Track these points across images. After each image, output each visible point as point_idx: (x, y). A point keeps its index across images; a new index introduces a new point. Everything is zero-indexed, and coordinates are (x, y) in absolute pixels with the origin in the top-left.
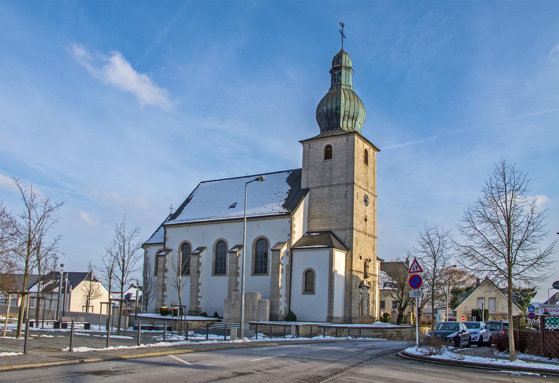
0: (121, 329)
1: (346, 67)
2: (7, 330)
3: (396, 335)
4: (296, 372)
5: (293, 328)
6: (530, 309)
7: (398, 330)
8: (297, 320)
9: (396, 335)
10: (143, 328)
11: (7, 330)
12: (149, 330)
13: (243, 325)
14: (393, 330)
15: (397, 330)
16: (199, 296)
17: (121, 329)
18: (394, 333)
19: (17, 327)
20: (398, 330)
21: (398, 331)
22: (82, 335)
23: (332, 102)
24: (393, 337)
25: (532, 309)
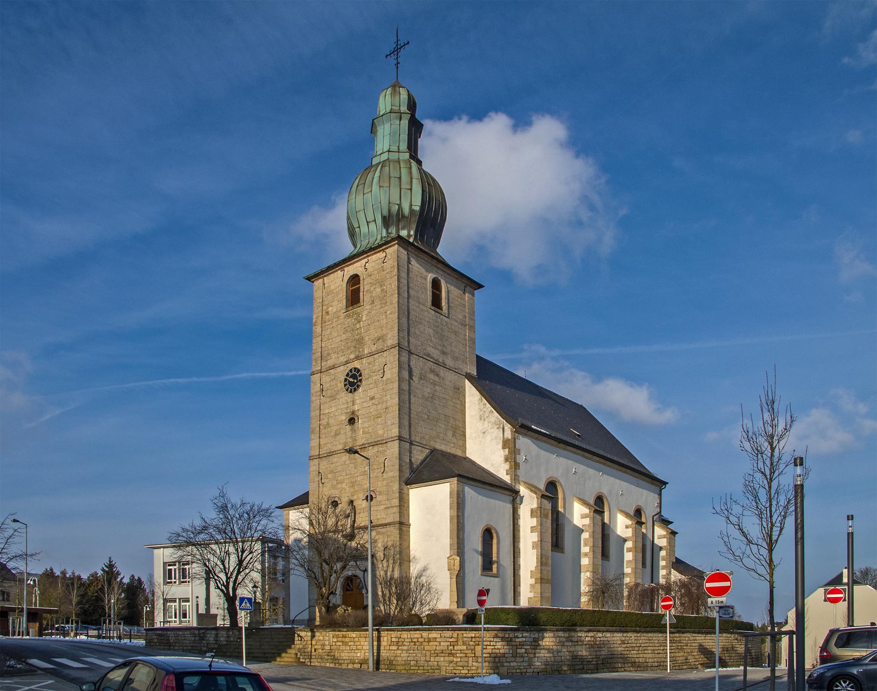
0: (111, 635)
1: (400, 151)
2: (187, 568)
3: (156, 640)
4: (445, 637)
5: (719, 570)
6: (243, 605)
7: (160, 632)
8: (29, 623)
9: (156, 640)
10: (110, 634)
11: (187, 568)
12: (284, 625)
13: (28, 637)
14: (153, 632)
15: (158, 632)
16: (665, 561)
17: (111, 635)
18: (153, 637)
19: (787, 672)
20: (160, 632)
21: (159, 635)
22: (580, 595)
23: (364, 192)
24: (153, 644)
25: (248, 605)
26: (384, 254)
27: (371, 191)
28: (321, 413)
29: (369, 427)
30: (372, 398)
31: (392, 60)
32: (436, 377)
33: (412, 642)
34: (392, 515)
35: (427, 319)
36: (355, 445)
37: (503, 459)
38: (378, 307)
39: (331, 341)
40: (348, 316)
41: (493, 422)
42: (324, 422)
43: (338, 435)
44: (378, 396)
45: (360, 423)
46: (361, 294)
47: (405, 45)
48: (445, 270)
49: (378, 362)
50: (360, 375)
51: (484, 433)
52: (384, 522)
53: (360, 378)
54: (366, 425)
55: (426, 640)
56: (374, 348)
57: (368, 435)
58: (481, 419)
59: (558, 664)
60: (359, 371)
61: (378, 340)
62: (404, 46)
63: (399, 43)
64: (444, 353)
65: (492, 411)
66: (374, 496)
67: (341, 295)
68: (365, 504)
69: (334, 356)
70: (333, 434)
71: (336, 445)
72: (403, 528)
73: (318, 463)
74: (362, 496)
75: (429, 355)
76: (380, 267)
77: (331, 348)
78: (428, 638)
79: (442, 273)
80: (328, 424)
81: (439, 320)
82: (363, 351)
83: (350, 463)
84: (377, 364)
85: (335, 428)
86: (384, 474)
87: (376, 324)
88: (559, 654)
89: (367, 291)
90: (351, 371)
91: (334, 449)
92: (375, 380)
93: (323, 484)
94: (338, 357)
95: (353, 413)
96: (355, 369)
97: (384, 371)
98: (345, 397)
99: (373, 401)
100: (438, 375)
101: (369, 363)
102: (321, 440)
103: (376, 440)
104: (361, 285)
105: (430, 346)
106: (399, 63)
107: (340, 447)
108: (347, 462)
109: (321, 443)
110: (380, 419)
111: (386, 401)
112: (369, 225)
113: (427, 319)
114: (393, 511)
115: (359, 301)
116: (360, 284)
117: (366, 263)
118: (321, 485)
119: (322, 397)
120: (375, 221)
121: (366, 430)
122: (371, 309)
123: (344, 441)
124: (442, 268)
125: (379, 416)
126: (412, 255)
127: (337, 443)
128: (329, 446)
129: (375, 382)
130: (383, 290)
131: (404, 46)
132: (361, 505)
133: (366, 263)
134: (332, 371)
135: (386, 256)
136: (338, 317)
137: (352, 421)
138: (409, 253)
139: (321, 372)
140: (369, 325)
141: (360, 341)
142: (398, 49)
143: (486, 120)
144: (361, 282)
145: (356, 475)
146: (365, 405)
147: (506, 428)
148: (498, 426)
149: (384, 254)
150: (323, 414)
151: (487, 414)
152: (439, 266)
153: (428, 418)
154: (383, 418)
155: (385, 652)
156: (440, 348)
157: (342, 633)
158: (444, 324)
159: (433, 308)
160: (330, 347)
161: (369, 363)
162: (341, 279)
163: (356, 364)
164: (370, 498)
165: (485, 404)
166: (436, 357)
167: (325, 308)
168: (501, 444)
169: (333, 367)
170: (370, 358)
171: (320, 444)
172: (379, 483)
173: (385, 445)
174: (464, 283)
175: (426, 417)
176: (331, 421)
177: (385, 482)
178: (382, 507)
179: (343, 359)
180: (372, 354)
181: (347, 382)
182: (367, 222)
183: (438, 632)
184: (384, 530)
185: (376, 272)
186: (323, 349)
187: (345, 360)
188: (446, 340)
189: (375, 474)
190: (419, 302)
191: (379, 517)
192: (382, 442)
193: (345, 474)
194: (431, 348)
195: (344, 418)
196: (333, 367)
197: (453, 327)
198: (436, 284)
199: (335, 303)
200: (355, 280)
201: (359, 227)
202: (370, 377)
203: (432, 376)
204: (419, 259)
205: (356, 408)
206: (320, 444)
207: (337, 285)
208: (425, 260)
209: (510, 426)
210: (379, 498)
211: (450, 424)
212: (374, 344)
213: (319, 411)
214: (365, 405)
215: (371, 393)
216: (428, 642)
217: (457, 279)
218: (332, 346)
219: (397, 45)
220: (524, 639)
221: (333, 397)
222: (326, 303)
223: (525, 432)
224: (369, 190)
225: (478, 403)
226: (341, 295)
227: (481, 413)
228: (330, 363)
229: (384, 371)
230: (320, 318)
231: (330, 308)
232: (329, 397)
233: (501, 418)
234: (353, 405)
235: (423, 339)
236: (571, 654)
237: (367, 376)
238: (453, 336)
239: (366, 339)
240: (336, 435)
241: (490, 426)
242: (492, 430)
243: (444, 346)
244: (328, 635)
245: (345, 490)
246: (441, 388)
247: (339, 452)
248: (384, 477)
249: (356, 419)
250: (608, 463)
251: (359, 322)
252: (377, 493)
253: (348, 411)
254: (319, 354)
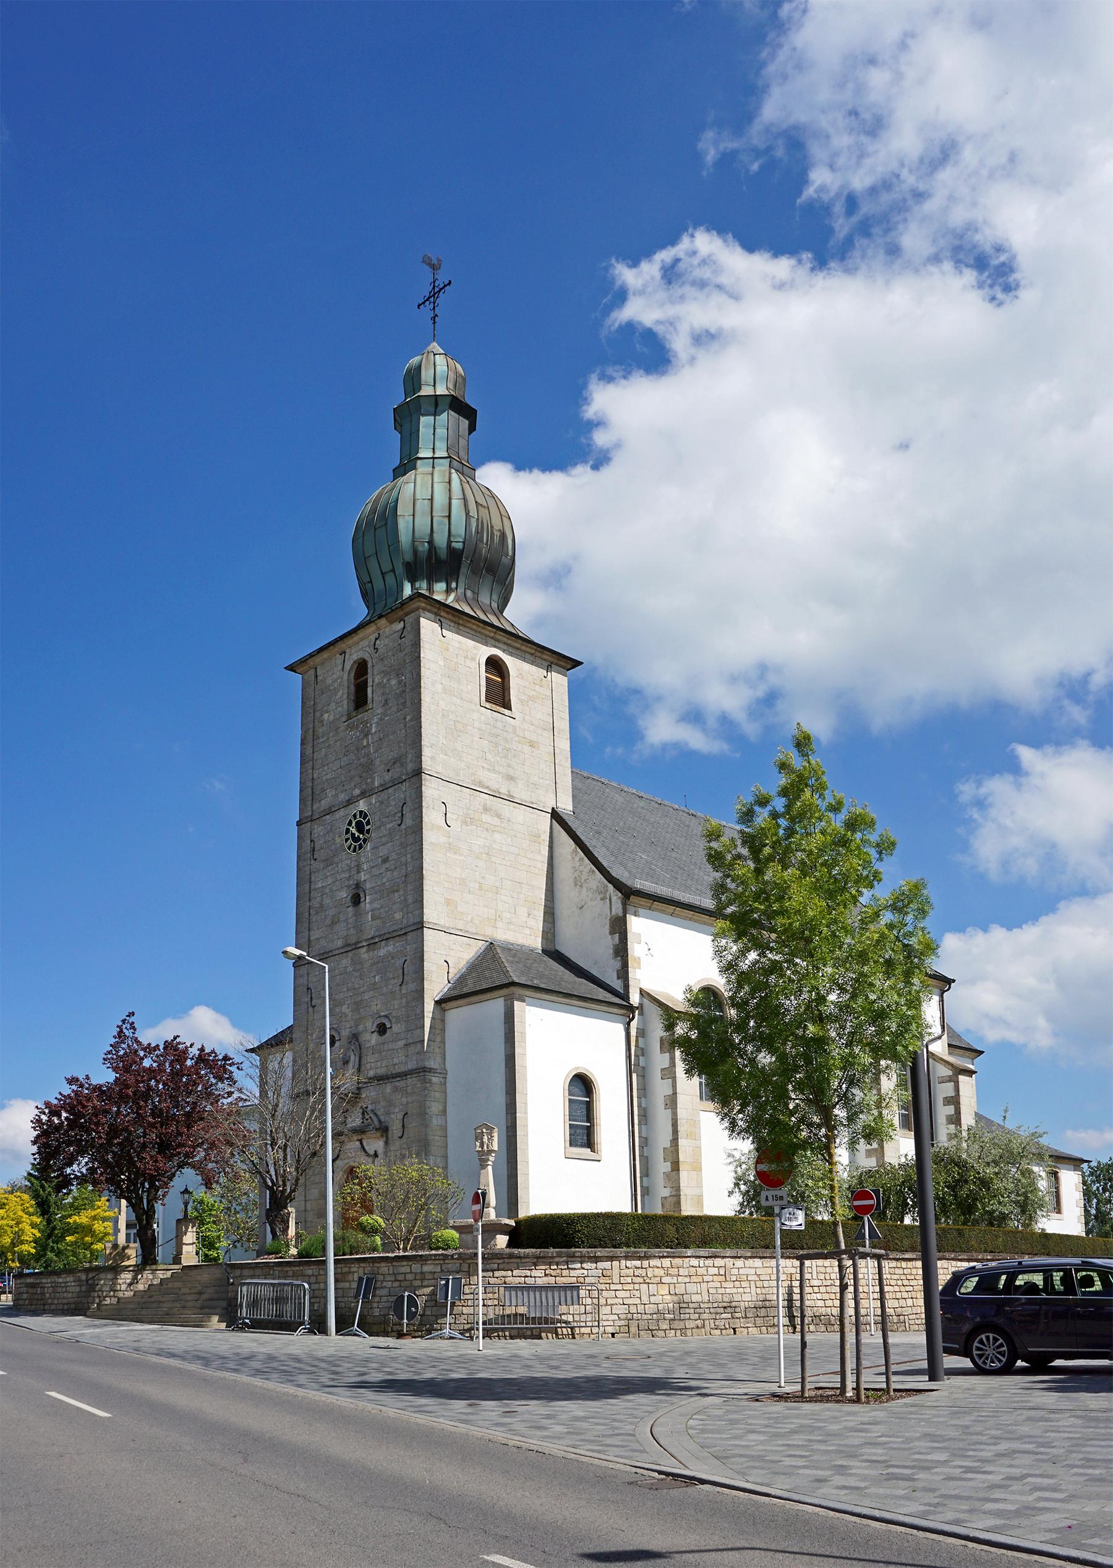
26: (402, 624)
27: (386, 524)
28: (312, 887)
29: (382, 907)
30: (385, 860)
31: (427, 311)
32: (496, 819)
33: (396, 1280)
34: (414, 1058)
35: (476, 724)
36: (360, 939)
37: (611, 951)
38: (394, 709)
39: (326, 768)
40: (351, 727)
41: (595, 888)
42: (315, 903)
43: (336, 923)
44: (394, 856)
45: (367, 903)
46: (369, 690)
47: (445, 286)
48: (509, 642)
49: (394, 800)
50: (368, 823)
51: (581, 908)
52: (403, 1069)
53: (367, 828)
54: (376, 905)
55: (418, 1277)
56: (387, 777)
57: (378, 922)
58: (576, 885)
59: (650, 1317)
60: (366, 816)
61: (394, 763)
62: (443, 288)
63: (436, 285)
64: (511, 778)
65: (593, 871)
66: (388, 1026)
67: (340, 693)
68: (374, 1039)
69: (330, 793)
70: (328, 922)
71: (332, 942)
72: (433, 1078)
73: (306, 972)
74: (371, 1025)
75: (481, 784)
76: (396, 645)
77: (327, 780)
78: (421, 1273)
79: (505, 647)
80: (321, 905)
81: (499, 725)
82: (373, 782)
83: (354, 970)
84: (393, 803)
85: (331, 912)
86: (404, 987)
87: (391, 737)
88: (653, 1299)
89: (378, 684)
90: (355, 816)
91: (331, 946)
92: (390, 829)
93: (314, 1007)
94: (336, 795)
95: (358, 886)
96: (361, 812)
97: (402, 815)
98: (346, 859)
99: (387, 865)
100: (499, 816)
101: (382, 803)
102: (312, 933)
103: (391, 929)
104: (369, 675)
105: (483, 767)
106: (437, 315)
107: (340, 943)
108: (350, 969)
109: (312, 938)
110: (396, 894)
111: (406, 864)
112: (386, 578)
113: (476, 724)
114: (417, 1050)
115: (366, 703)
116: (367, 674)
117: (376, 639)
118: (311, 1009)
119: (313, 862)
120: (393, 570)
121: (377, 912)
122: (385, 714)
123: (345, 933)
124: (505, 640)
125: (395, 888)
126: (447, 621)
127: (336, 937)
128: (323, 942)
129: (390, 833)
130: (400, 682)
131: (443, 288)
132: (369, 1041)
133: (376, 639)
134: (328, 817)
135: (404, 628)
136: (337, 729)
137: (356, 900)
138: (442, 620)
139: (311, 821)
140: (380, 739)
141: (368, 767)
142: (434, 295)
143: (650, 377)
144: (370, 671)
145: (362, 990)
146: (375, 871)
147: (614, 899)
148: (602, 896)
149: (402, 624)
150: (315, 890)
151: (584, 876)
152: (497, 636)
153: (481, 889)
154: (401, 892)
155: (588, 1280)
156: (502, 770)
157: (294, 1269)
158: (510, 730)
159: (488, 705)
160: (324, 778)
161: (382, 803)
162: (340, 667)
163: (362, 805)
164: (382, 1029)
165: (581, 859)
166: (494, 786)
167: (318, 714)
168: (608, 926)
169: (330, 811)
170: (382, 794)
171: (309, 940)
172: (396, 1002)
173: (404, 937)
174: (545, 660)
175: (477, 886)
176: (327, 901)
177: (404, 1000)
178: (401, 1043)
179: (343, 797)
180: (384, 788)
181: (349, 835)
182: (382, 573)
183: (437, 1262)
184: (401, 1084)
185: (390, 653)
186: (316, 783)
187: (347, 798)
188: (514, 756)
189: (390, 987)
190: (462, 699)
191: (396, 1061)
192: (400, 933)
193: (345, 989)
194: (486, 772)
195: (344, 894)
196: (330, 811)
197: (527, 734)
198: (494, 665)
199: (333, 706)
200: (361, 668)
201: (371, 582)
202: (383, 824)
203: (486, 818)
204: (461, 628)
205: (363, 877)
206: (309, 940)
207: (334, 676)
208: (471, 629)
209: (620, 894)
210: (396, 1028)
211: (522, 896)
212: (388, 771)
213: (308, 885)
214: (375, 871)
215: (383, 851)
216: (422, 1280)
217: (532, 654)
218: (329, 776)
219: (434, 288)
220: (585, 1272)
221: (329, 862)
222: (319, 706)
223: (649, 905)
224: (384, 523)
225: (570, 857)
226: (340, 693)
227: (576, 875)
228: (324, 804)
229: (402, 815)
230: (311, 731)
231: (326, 716)
232: (323, 861)
233: (606, 882)
234: (359, 872)
235: (470, 757)
236: (676, 1299)
237: (378, 824)
238: (527, 749)
239: (377, 762)
240: (334, 923)
241: (590, 895)
242: (594, 903)
243: (509, 766)
244: (271, 1272)
245: (346, 1016)
246: (505, 836)
247: (337, 952)
248: (404, 992)
249: (362, 895)
250: (488, 996)
251: (366, 735)
252: (393, 1020)
253: (351, 882)
254: (309, 790)
